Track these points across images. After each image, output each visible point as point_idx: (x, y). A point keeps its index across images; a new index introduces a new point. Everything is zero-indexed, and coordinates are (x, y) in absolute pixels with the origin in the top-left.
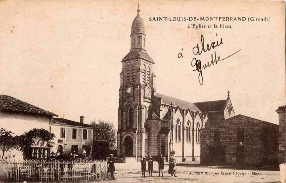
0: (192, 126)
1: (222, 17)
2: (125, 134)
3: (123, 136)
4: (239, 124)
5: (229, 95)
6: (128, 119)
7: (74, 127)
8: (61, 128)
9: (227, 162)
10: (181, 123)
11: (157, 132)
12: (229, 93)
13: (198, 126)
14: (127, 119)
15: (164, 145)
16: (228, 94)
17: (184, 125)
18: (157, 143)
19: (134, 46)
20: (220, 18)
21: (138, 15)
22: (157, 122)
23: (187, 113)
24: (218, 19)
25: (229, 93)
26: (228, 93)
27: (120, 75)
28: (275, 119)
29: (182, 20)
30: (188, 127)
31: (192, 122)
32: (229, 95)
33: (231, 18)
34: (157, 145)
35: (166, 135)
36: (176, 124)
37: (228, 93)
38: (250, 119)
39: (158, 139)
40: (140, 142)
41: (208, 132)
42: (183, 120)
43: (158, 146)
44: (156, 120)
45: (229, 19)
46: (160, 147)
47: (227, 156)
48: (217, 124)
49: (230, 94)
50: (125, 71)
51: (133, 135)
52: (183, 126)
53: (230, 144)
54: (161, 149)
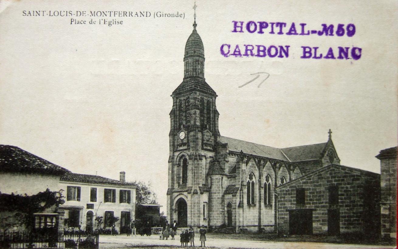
0: (274, 182)
1: (113, 11)
2: (177, 196)
3: (175, 198)
4: (332, 178)
5: (330, 136)
6: (181, 175)
7: (70, 183)
8: (105, 190)
9: (314, 232)
10: (272, 181)
11: (221, 192)
12: (330, 132)
13: (267, 180)
14: (179, 175)
15: (231, 210)
16: (328, 134)
17: (260, 181)
18: (221, 207)
19: (187, 74)
20: (84, 13)
21: (195, 22)
22: (221, 178)
23: (280, 166)
24: (113, 14)
25: (330, 132)
26: (329, 133)
27: (170, 114)
28: (374, 167)
29: (115, 24)
30: (267, 184)
31: (274, 176)
32: (330, 136)
33: (125, 13)
34: (221, 210)
35: (233, 196)
36: (265, 181)
37: (329, 133)
38: (348, 169)
39: (223, 201)
40: (196, 206)
41: (289, 190)
42: (276, 176)
43: (222, 211)
44: (220, 175)
45: (128, 14)
46: (226, 213)
47: (315, 225)
48: (300, 179)
49: (332, 134)
50: (177, 108)
51: (187, 197)
52: (260, 182)
53: (318, 207)
54: (226, 215)
